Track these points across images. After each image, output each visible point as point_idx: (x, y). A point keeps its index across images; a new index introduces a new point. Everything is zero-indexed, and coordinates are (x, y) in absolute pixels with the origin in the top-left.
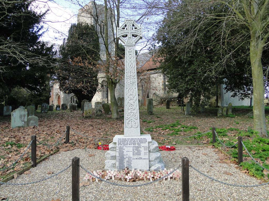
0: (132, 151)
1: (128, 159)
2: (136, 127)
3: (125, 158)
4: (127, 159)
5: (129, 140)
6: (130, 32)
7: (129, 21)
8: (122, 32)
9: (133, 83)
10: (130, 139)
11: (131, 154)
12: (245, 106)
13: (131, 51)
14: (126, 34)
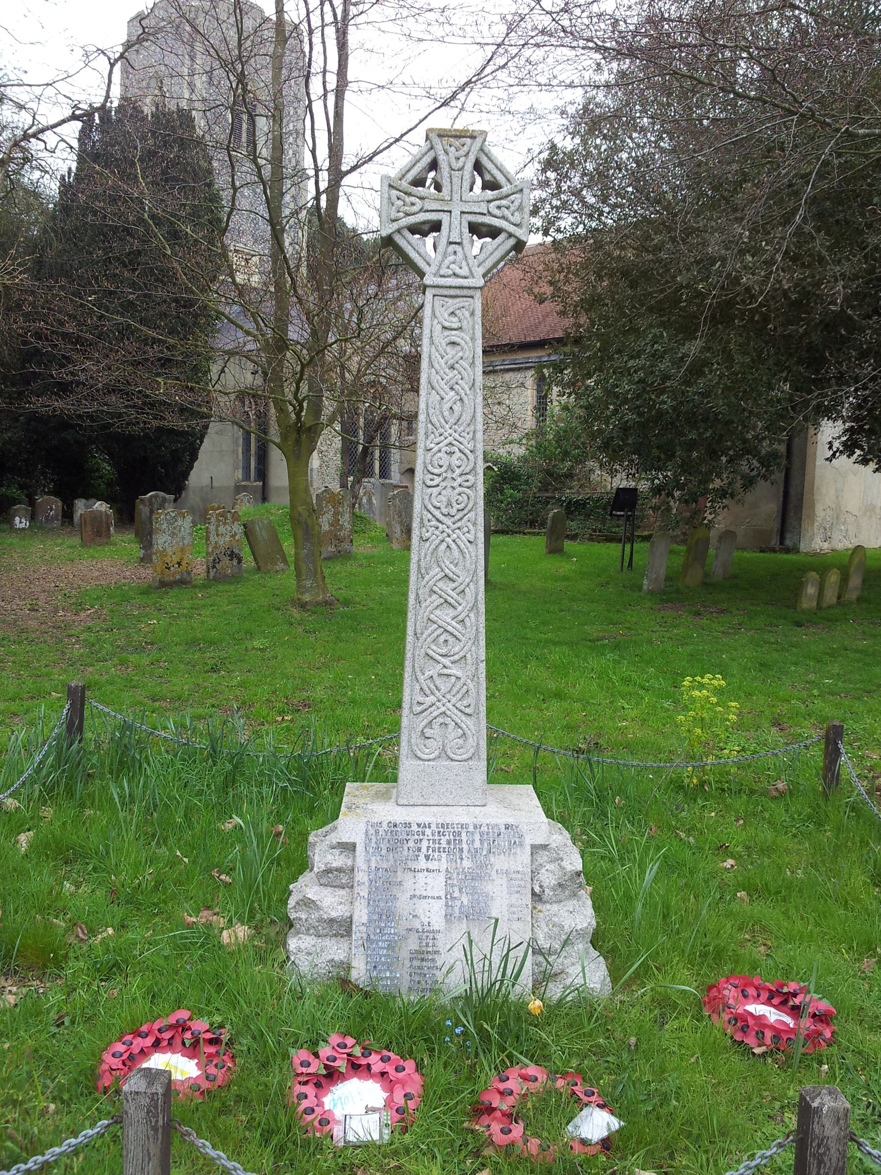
0: (439, 898)
1: (417, 941)
8: (413, 204)
13: (455, 326)
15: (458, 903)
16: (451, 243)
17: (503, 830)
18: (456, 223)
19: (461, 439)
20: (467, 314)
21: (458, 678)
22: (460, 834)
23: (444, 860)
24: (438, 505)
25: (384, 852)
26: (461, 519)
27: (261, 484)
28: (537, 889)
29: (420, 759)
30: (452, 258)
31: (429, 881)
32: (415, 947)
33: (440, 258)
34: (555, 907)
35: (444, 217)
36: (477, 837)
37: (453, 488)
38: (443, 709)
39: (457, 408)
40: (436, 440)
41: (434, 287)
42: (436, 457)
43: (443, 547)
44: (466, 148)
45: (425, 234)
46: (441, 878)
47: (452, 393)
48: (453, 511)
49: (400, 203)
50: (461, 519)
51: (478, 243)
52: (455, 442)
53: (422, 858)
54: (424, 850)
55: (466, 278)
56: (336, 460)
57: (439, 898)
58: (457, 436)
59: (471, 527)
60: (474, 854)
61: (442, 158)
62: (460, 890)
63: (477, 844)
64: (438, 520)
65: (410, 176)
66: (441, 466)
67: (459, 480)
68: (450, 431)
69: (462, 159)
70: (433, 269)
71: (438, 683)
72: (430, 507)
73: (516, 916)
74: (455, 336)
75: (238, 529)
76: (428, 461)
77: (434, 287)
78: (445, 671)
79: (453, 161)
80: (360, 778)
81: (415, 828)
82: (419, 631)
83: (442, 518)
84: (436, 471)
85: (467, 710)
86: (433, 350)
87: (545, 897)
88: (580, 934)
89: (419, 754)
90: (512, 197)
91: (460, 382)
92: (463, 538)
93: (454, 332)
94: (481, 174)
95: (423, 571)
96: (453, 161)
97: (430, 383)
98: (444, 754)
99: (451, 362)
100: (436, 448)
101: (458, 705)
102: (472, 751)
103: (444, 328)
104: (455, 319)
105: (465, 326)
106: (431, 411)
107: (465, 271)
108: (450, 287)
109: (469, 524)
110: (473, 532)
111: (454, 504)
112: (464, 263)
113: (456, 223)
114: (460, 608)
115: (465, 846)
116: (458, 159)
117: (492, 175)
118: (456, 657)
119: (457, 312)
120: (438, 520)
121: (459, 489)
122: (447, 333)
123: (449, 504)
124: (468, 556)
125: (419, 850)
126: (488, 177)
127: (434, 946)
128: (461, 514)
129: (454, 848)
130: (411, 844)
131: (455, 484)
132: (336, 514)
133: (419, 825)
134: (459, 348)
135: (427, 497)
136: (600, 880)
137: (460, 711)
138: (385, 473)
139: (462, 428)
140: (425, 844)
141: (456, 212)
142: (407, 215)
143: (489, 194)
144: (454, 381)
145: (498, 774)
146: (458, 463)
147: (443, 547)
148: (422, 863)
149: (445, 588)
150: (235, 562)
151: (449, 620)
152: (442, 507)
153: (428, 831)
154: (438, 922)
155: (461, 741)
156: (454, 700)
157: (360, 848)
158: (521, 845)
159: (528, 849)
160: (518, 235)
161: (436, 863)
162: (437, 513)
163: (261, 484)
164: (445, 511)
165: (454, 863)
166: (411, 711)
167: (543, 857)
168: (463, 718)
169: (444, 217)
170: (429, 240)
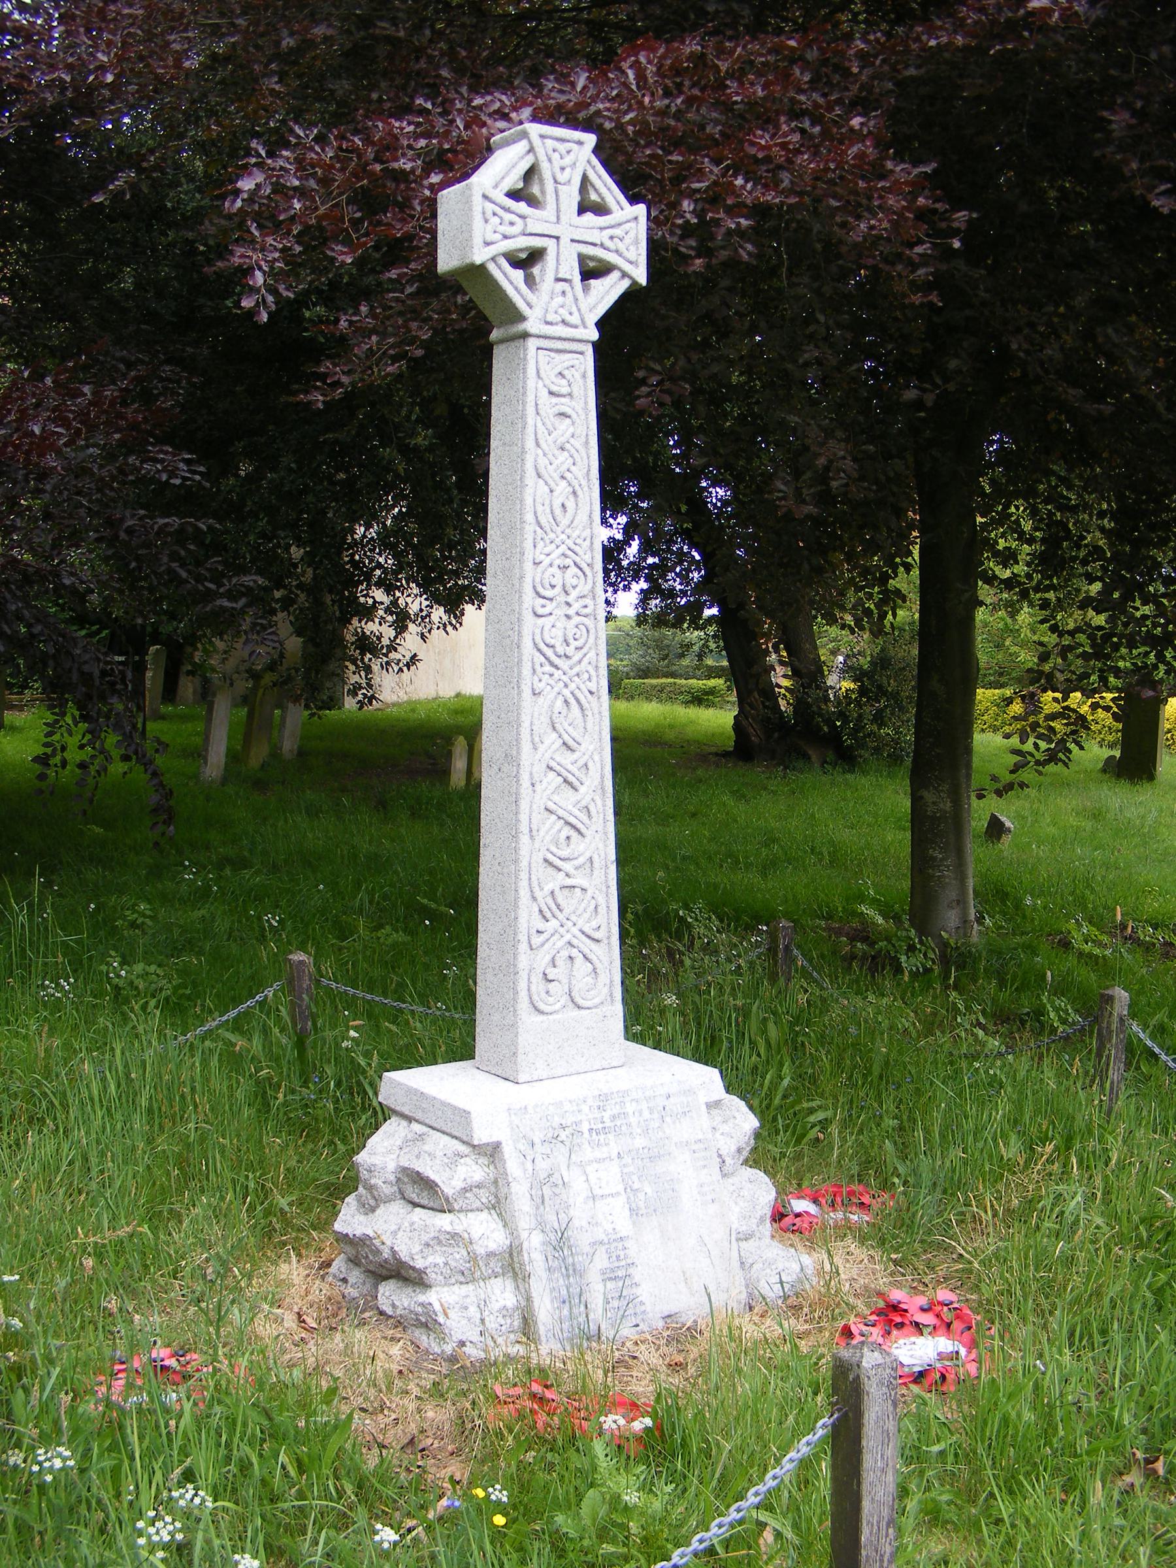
0: (618, 1193)
1: (605, 1256)
2: (535, 997)
3: (587, 1249)
4: (601, 1262)
5: (585, 1108)
6: (566, 235)
7: (557, 145)
8: (512, 224)
9: (580, 654)
10: (590, 1102)
11: (615, 1216)
12: (471, 697)
13: (565, 390)
14: (537, 242)
16: (558, 280)
19: (577, 549)
20: (578, 375)
24: (552, 642)
26: (580, 662)
29: (542, 1012)
30: (560, 300)
32: (605, 1264)
37: (568, 617)
39: (570, 505)
40: (547, 550)
41: (539, 337)
42: (547, 574)
44: (572, 156)
47: (564, 483)
48: (570, 651)
49: (496, 220)
50: (580, 662)
52: (569, 553)
55: (576, 327)
58: (570, 543)
59: (593, 673)
61: (544, 166)
64: (552, 664)
66: (553, 587)
67: (576, 606)
68: (564, 537)
69: (568, 170)
71: (560, 900)
72: (542, 646)
73: (709, 1198)
76: (538, 580)
77: (539, 337)
78: (569, 882)
79: (557, 170)
82: (534, 827)
83: (557, 661)
85: (596, 935)
86: (539, 424)
89: (542, 1006)
90: (627, 226)
91: (573, 468)
92: (582, 687)
93: (563, 400)
95: (537, 739)
96: (557, 170)
99: (561, 440)
100: (547, 561)
101: (586, 929)
103: (551, 393)
104: (564, 382)
105: (575, 393)
106: (540, 509)
108: (560, 339)
110: (594, 679)
111: (571, 641)
112: (574, 309)
114: (583, 789)
116: (563, 169)
117: (599, 195)
119: (566, 372)
120: (552, 664)
122: (554, 400)
124: (589, 713)
127: (626, 1257)
128: (580, 654)
131: (571, 612)
137: (589, 937)
139: (577, 532)
142: (505, 237)
144: (565, 467)
146: (574, 581)
149: (563, 762)
151: (570, 807)
152: (558, 645)
153: (585, 1108)
154: (624, 1226)
156: (580, 923)
157: (508, 1150)
160: (634, 275)
161: (605, 1149)
162: (549, 652)
164: (560, 650)
165: (582, 1172)
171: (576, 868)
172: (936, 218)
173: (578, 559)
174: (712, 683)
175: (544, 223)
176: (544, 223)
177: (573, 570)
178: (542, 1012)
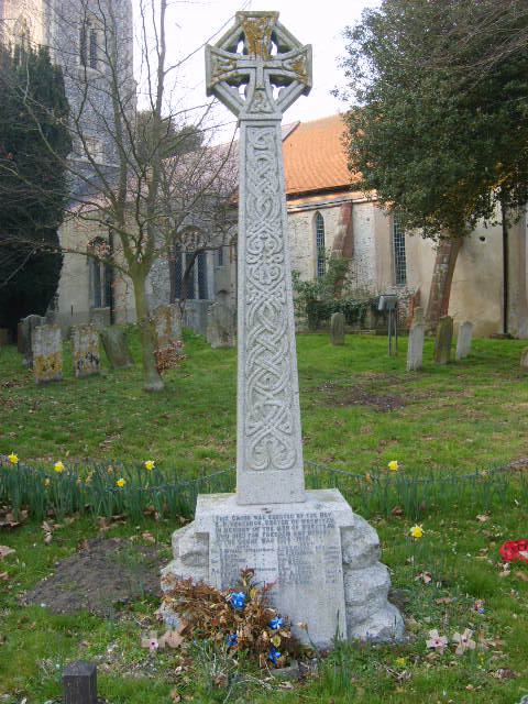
0: (274, 569)
15: (289, 572)
17: (319, 518)
18: (260, 76)
21: (279, 407)
22: (286, 522)
23: (276, 542)
25: (231, 538)
27: (109, 308)
28: (346, 559)
29: (283, 248)
31: (266, 557)
33: (250, 100)
34: (361, 572)
35: (252, 72)
36: (300, 524)
37: (268, 257)
38: (268, 431)
43: (262, 308)
45: (238, 85)
46: (275, 554)
51: (276, 90)
53: (259, 541)
54: (261, 535)
56: (167, 286)
57: (274, 569)
60: (299, 536)
62: (290, 562)
63: (300, 529)
65: (225, 45)
70: (245, 108)
74: (263, 154)
75: (96, 337)
78: (270, 402)
80: (203, 492)
81: (252, 519)
84: (255, 252)
87: (352, 565)
88: (380, 590)
89: (253, 466)
94: (276, 43)
97: (246, 188)
98: (270, 464)
102: (293, 461)
107: (268, 109)
109: (282, 290)
113: (260, 76)
115: (291, 531)
118: (277, 391)
121: (272, 265)
122: (258, 152)
123: (265, 276)
125: (257, 535)
126: (281, 43)
128: (275, 283)
129: (283, 535)
130: (251, 531)
132: (169, 323)
133: (255, 517)
134: (266, 163)
135: (248, 272)
136: (390, 553)
138: (203, 295)
140: (261, 531)
141: (260, 68)
143: (283, 56)
145: (313, 482)
147: (262, 308)
148: (260, 545)
150: (94, 363)
155: (283, 454)
158: (333, 527)
159: (338, 530)
162: (256, 283)
163: (109, 308)
164: (263, 281)
166: (245, 434)
167: (349, 536)
168: (285, 437)
169: (252, 72)
170: (242, 88)
171: (274, 395)
172: (114, 336)
173: (273, 233)
174: (210, 321)
175: (278, 525)
176: (278, 525)
177: (270, 239)
178: (283, 248)
